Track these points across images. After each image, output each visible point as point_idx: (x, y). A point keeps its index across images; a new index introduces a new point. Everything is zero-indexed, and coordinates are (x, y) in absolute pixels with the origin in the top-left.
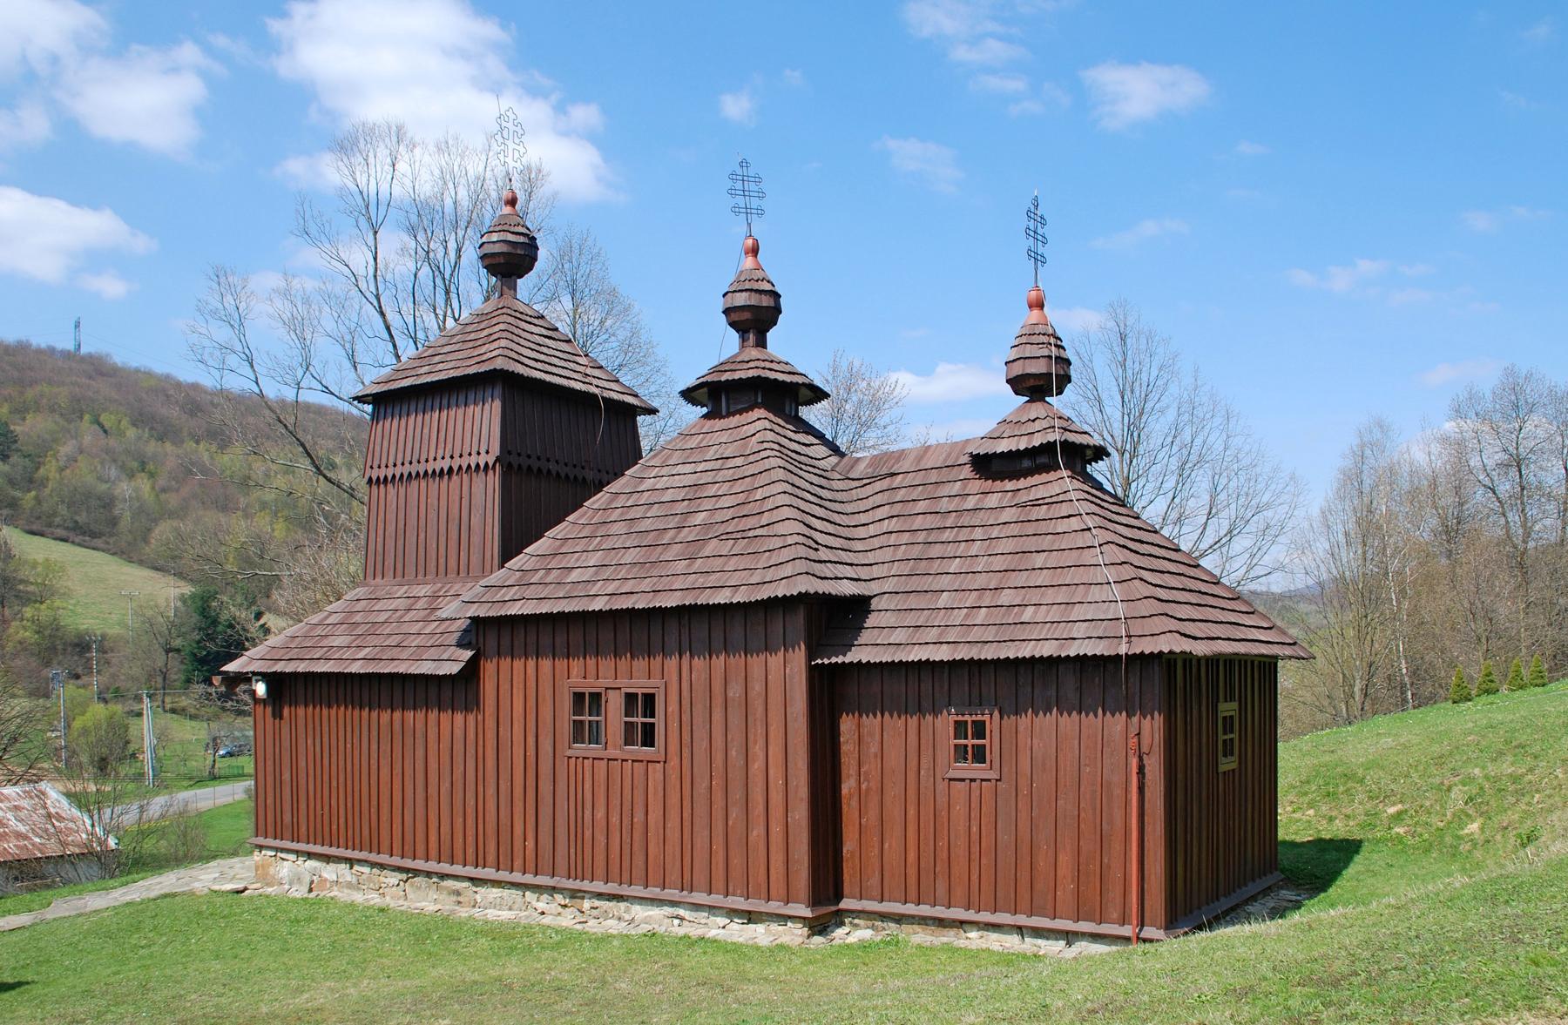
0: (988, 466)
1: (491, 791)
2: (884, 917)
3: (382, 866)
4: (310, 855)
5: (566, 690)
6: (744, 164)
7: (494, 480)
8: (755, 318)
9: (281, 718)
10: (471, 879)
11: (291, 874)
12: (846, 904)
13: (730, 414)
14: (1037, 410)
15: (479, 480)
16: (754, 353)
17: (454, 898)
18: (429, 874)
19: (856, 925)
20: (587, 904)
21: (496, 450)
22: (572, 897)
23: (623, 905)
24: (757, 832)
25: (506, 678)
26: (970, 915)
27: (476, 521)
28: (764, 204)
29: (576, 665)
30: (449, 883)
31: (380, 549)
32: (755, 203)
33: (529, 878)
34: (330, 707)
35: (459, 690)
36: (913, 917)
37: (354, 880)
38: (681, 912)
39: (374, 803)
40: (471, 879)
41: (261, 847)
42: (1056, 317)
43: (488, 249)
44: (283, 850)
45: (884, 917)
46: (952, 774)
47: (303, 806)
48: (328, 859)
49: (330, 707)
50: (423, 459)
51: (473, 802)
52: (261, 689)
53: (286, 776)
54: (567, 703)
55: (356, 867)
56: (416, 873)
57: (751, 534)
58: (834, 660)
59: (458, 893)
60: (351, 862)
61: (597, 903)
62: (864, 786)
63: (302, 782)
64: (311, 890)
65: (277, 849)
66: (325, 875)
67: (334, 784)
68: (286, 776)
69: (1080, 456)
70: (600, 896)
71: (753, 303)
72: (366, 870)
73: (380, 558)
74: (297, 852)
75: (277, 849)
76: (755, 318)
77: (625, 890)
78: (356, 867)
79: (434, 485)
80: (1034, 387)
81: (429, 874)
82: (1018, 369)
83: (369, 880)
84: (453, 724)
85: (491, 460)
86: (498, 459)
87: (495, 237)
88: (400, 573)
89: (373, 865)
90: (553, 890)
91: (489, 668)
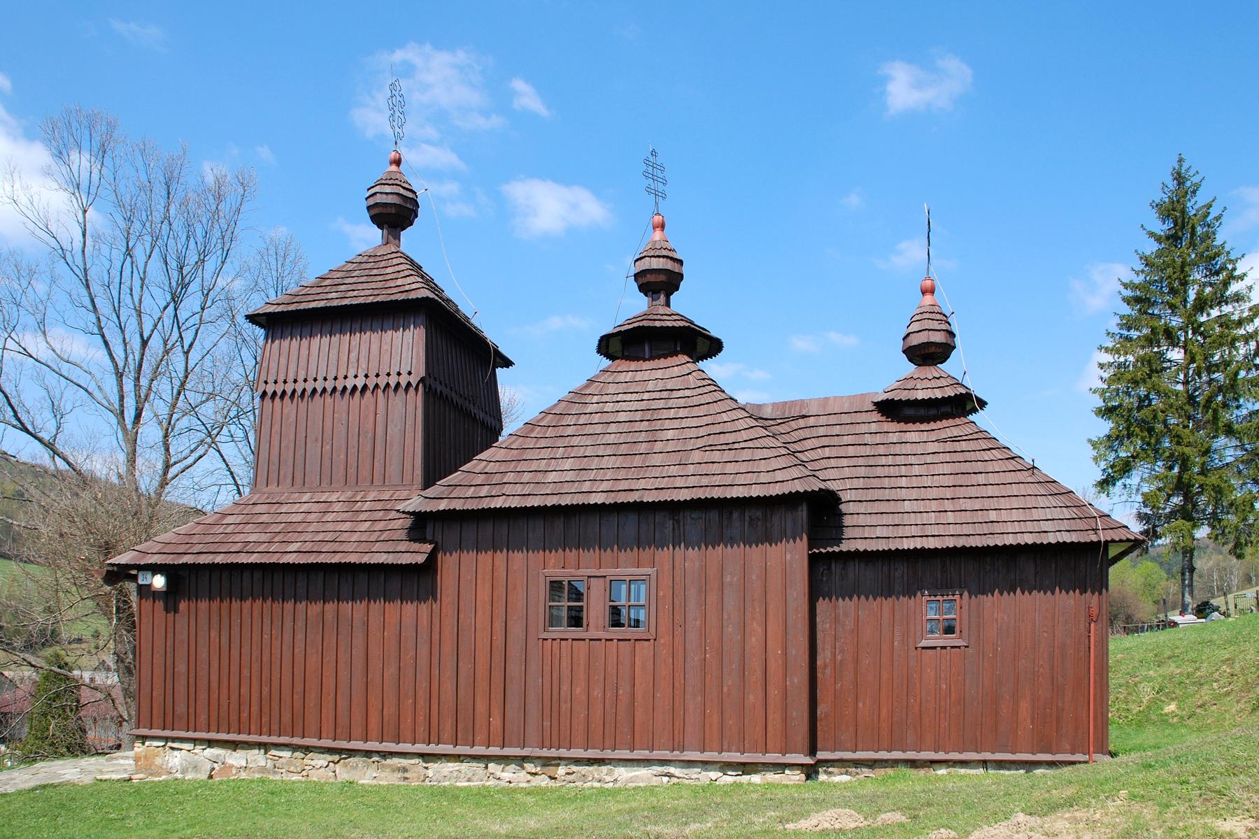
0: (891, 409)
1: (449, 673)
2: (858, 763)
3: (307, 749)
4: (211, 743)
5: (542, 579)
6: (654, 153)
7: (416, 401)
8: (660, 282)
9: (176, 611)
10: (422, 756)
11: (181, 761)
12: (821, 755)
13: (652, 358)
14: (930, 372)
15: (397, 400)
16: (662, 310)
17: (400, 775)
18: (368, 754)
19: (830, 773)
20: (561, 771)
21: (420, 371)
22: (544, 765)
23: (605, 769)
24: (753, 698)
25: (463, 570)
26: (941, 756)
27: (394, 431)
28: (667, 189)
29: (554, 557)
30: (396, 761)
31: (275, 459)
32: (661, 187)
33: (494, 751)
34: (264, 600)
35: (414, 581)
36: (886, 761)
37: (270, 764)
38: (672, 770)
39: (299, 688)
40: (422, 756)
41: (144, 738)
42: (944, 300)
43: (379, 199)
44: (174, 740)
45: (858, 763)
46: (924, 643)
47: (202, 696)
48: (234, 745)
49: (264, 600)
50: (281, 379)
51: (425, 685)
52: (159, 582)
53: (181, 667)
54: (542, 591)
55: (273, 752)
56: (352, 753)
57: (736, 446)
58: (830, 550)
59: (405, 770)
60: (265, 747)
61: (574, 768)
62: (839, 657)
63: (202, 673)
64: (211, 777)
65: (166, 739)
66: (230, 761)
67: (246, 672)
68: (181, 667)
69: (962, 404)
70: (577, 761)
71: (669, 267)
72: (286, 754)
73: (274, 468)
74: (195, 741)
75: (166, 739)
76: (660, 282)
77: (608, 754)
78: (147, 743)
79: (342, 403)
80: (927, 354)
81: (368, 754)
82: (915, 340)
83: (289, 763)
84: (407, 614)
85: (414, 380)
86: (422, 380)
87: (388, 189)
88: (299, 481)
89: (294, 748)
90: (523, 759)
91: (448, 563)
